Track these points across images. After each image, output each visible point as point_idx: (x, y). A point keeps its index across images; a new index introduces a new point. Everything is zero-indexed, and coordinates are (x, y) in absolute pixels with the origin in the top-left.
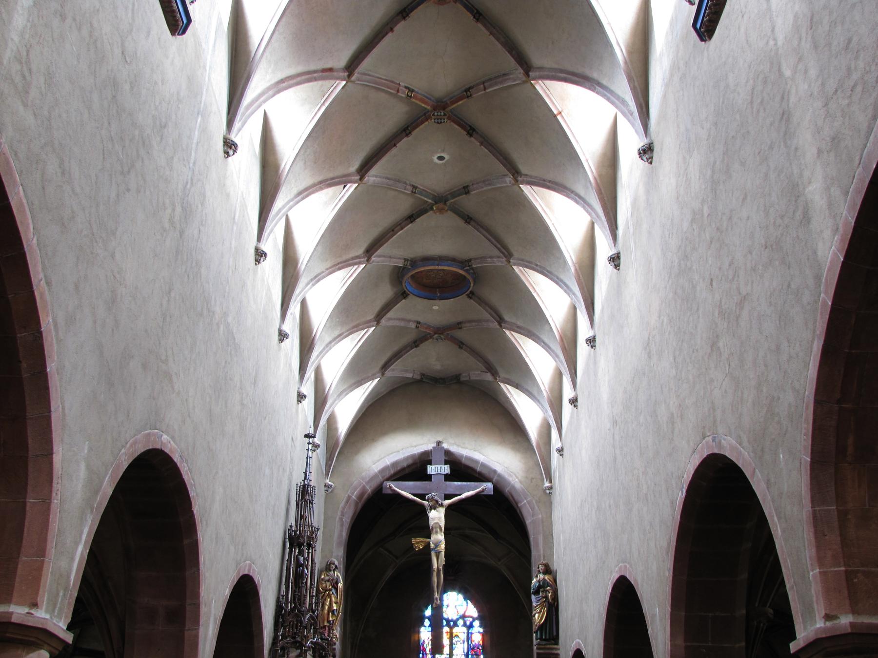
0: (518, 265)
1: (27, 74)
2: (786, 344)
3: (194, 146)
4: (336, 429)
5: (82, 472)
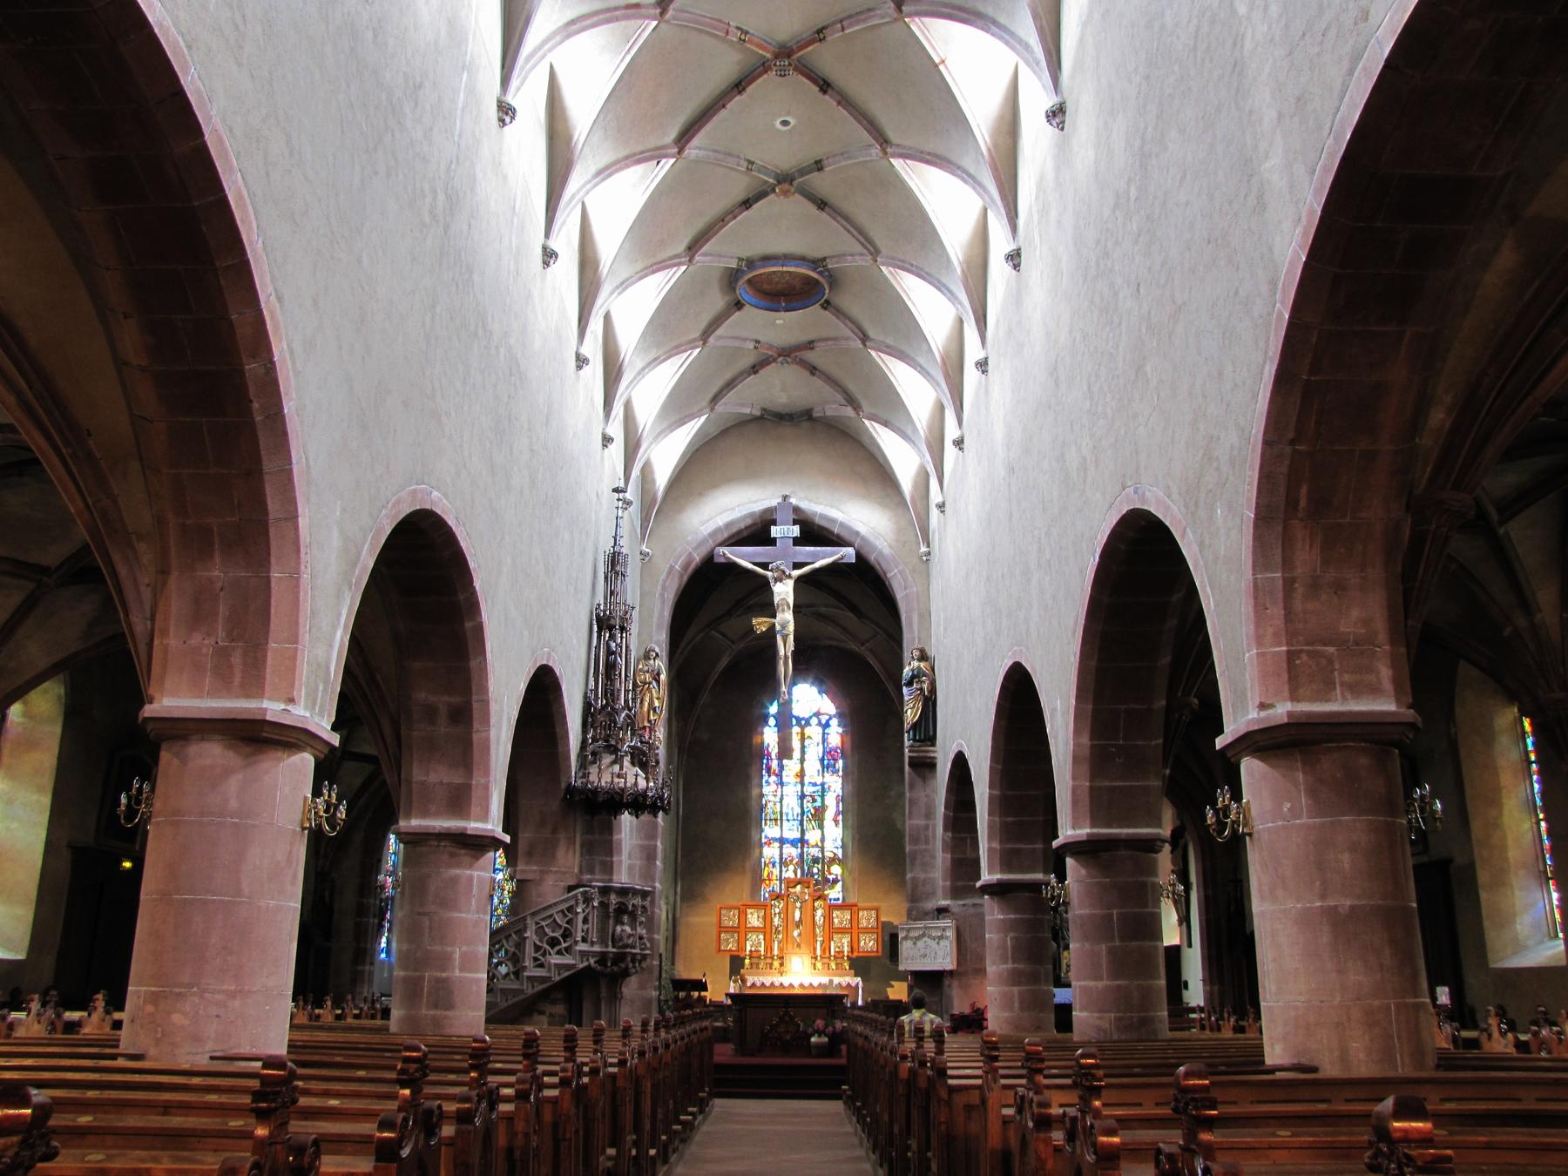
0: (888, 265)
1: (240, 23)
2: (1230, 368)
3: (459, 112)
4: (653, 481)
5: (336, 540)
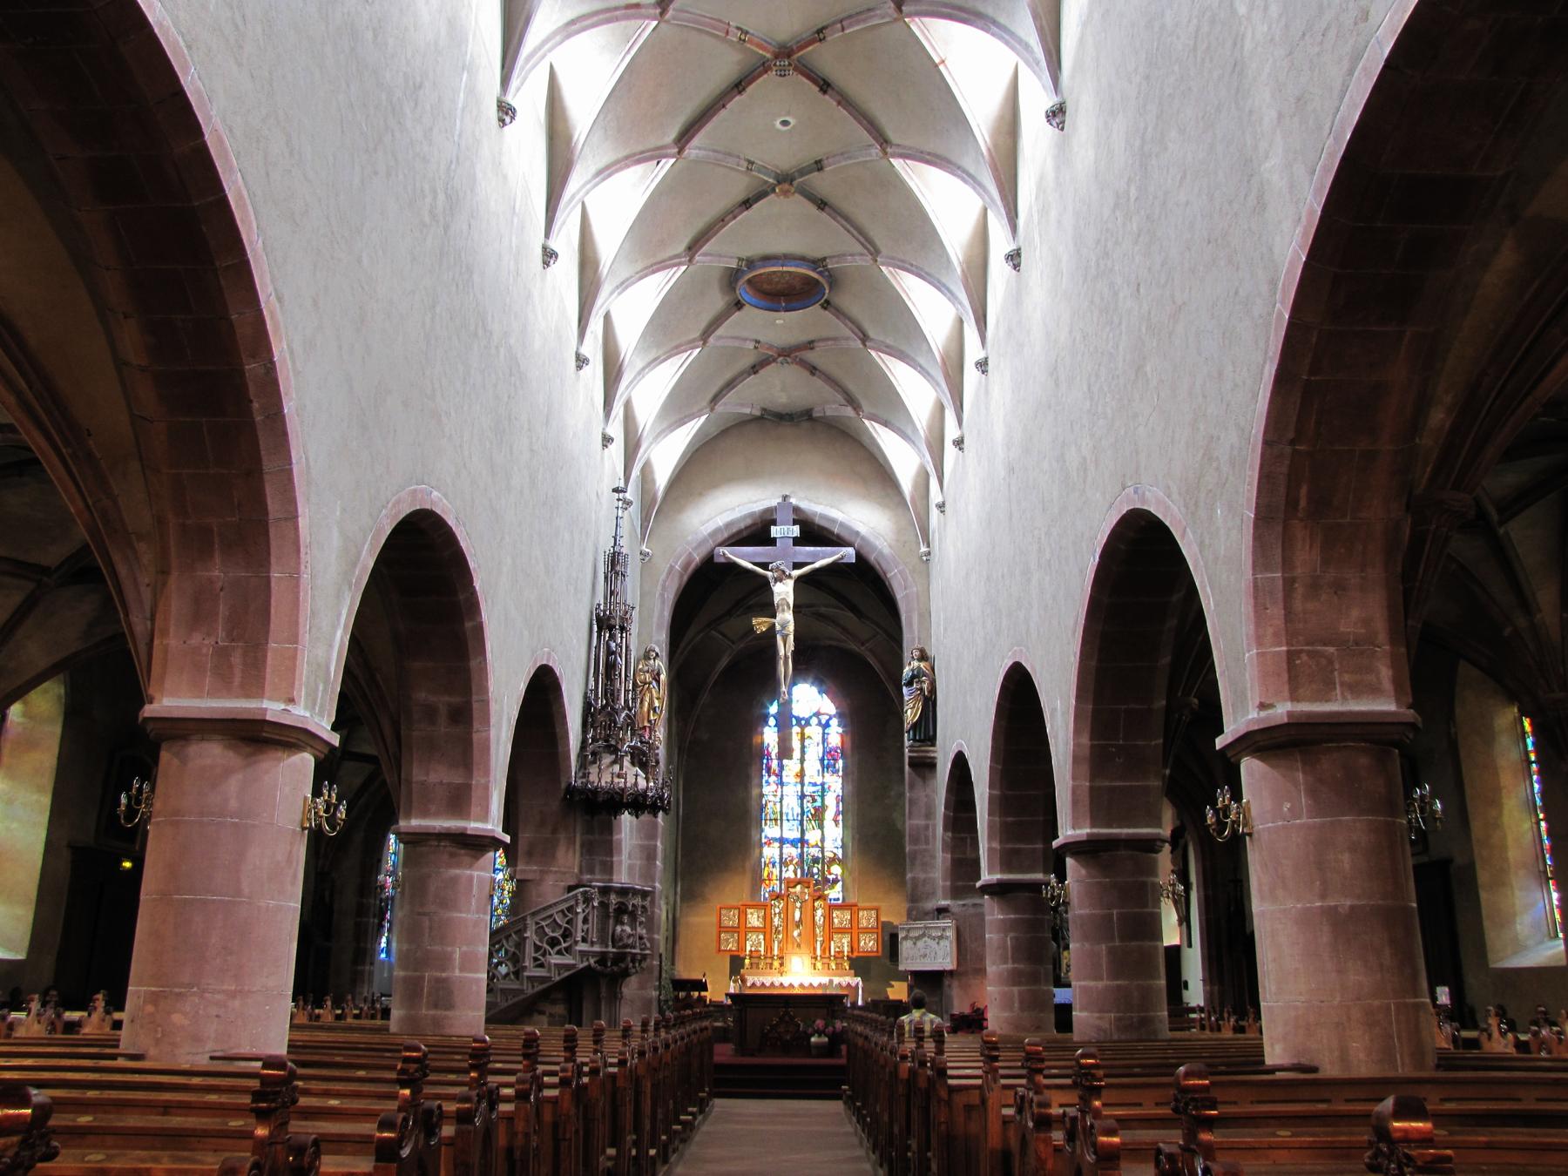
0: (888, 265)
1: (240, 23)
2: (1230, 368)
3: (459, 112)
4: (653, 481)
5: (336, 540)
